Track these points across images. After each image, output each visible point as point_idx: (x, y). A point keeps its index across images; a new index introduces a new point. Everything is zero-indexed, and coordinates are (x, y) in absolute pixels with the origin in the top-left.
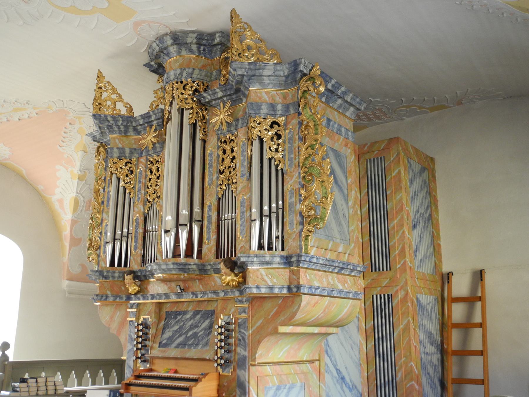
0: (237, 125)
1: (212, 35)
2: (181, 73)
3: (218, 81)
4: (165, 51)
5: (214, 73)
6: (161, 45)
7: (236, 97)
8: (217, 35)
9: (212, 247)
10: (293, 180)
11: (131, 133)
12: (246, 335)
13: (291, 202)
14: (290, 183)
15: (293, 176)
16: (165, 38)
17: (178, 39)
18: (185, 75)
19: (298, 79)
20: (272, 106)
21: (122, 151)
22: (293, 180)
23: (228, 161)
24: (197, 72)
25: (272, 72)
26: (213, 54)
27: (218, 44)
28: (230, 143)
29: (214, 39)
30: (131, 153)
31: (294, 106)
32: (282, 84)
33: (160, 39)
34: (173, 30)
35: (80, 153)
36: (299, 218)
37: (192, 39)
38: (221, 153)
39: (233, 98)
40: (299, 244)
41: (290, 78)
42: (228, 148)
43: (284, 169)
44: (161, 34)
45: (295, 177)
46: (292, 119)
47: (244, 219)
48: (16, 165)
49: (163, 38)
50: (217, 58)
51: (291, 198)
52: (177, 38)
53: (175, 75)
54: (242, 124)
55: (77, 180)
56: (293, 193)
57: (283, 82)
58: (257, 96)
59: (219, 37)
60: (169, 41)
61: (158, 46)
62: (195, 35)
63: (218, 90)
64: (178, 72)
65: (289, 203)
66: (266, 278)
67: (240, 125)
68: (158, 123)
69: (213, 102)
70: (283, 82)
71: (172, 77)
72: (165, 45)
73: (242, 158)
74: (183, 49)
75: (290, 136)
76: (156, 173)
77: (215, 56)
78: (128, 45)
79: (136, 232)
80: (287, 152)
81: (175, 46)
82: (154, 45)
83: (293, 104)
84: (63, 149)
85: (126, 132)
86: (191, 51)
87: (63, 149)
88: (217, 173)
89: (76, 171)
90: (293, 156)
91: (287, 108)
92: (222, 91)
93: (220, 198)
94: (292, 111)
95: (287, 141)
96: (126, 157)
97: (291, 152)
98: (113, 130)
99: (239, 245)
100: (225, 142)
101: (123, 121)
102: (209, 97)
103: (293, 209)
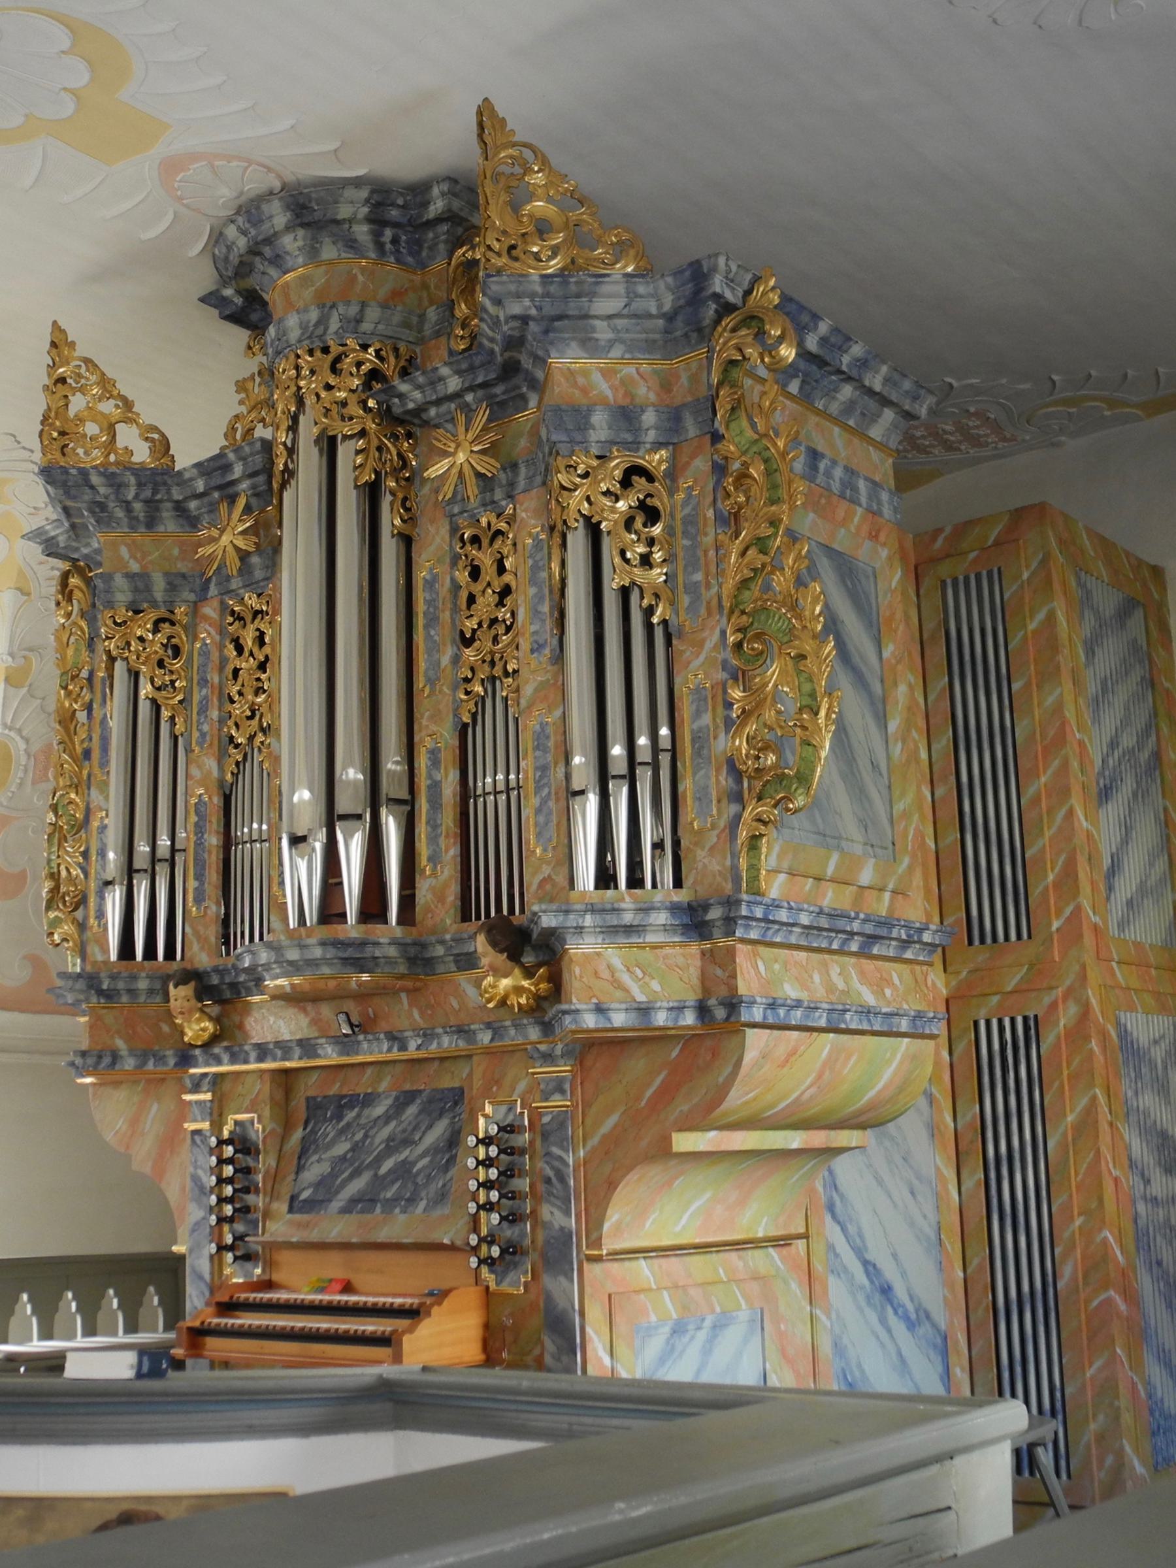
0: (512, 484)
1: (419, 191)
2: (323, 321)
6: (253, 232)
7: (503, 393)
8: (436, 191)
10: (702, 657)
11: (169, 523)
15: (701, 644)
16: (264, 207)
17: (308, 207)
19: (707, 322)
21: (140, 582)
22: (702, 657)
26: (424, 254)
27: (439, 220)
29: (425, 204)
30: (172, 587)
33: (250, 210)
34: (290, 178)
36: (725, 780)
38: (463, 576)
39: (496, 396)
41: (679, 322)
42: (486, 560)
45: (709, 645)
46: (693, 456)
47: (546, 791)
49: (258, 208)
50: (439, 264)
51: (698, 714)
52: (304, 207)
54: (530, 479)
58: (575, 384)
60: (279, 218)
61: (244, 233)
62: (364, 194)
64: (314, 315)
65: (692, 731)
66: (626, 978)
67: (522, 483)
68: (254, 487)
69: (433, 412)
70: (657, 336)
73: (532, 591)
75: (687, 510)
76: (256, 650)
77: (432, 258)
79: (199, 844)
80: (681, 564)
82: (231, 232)
85: (151, 523)
86: (351, 244)
90: (699, 577)
91: (673, 418)
92: (459, 372)
94: (691, 428)
97: (693, 564)
99: (534, 874)
100: (475, 540)
102: (417, 395)
103: (705, 752)
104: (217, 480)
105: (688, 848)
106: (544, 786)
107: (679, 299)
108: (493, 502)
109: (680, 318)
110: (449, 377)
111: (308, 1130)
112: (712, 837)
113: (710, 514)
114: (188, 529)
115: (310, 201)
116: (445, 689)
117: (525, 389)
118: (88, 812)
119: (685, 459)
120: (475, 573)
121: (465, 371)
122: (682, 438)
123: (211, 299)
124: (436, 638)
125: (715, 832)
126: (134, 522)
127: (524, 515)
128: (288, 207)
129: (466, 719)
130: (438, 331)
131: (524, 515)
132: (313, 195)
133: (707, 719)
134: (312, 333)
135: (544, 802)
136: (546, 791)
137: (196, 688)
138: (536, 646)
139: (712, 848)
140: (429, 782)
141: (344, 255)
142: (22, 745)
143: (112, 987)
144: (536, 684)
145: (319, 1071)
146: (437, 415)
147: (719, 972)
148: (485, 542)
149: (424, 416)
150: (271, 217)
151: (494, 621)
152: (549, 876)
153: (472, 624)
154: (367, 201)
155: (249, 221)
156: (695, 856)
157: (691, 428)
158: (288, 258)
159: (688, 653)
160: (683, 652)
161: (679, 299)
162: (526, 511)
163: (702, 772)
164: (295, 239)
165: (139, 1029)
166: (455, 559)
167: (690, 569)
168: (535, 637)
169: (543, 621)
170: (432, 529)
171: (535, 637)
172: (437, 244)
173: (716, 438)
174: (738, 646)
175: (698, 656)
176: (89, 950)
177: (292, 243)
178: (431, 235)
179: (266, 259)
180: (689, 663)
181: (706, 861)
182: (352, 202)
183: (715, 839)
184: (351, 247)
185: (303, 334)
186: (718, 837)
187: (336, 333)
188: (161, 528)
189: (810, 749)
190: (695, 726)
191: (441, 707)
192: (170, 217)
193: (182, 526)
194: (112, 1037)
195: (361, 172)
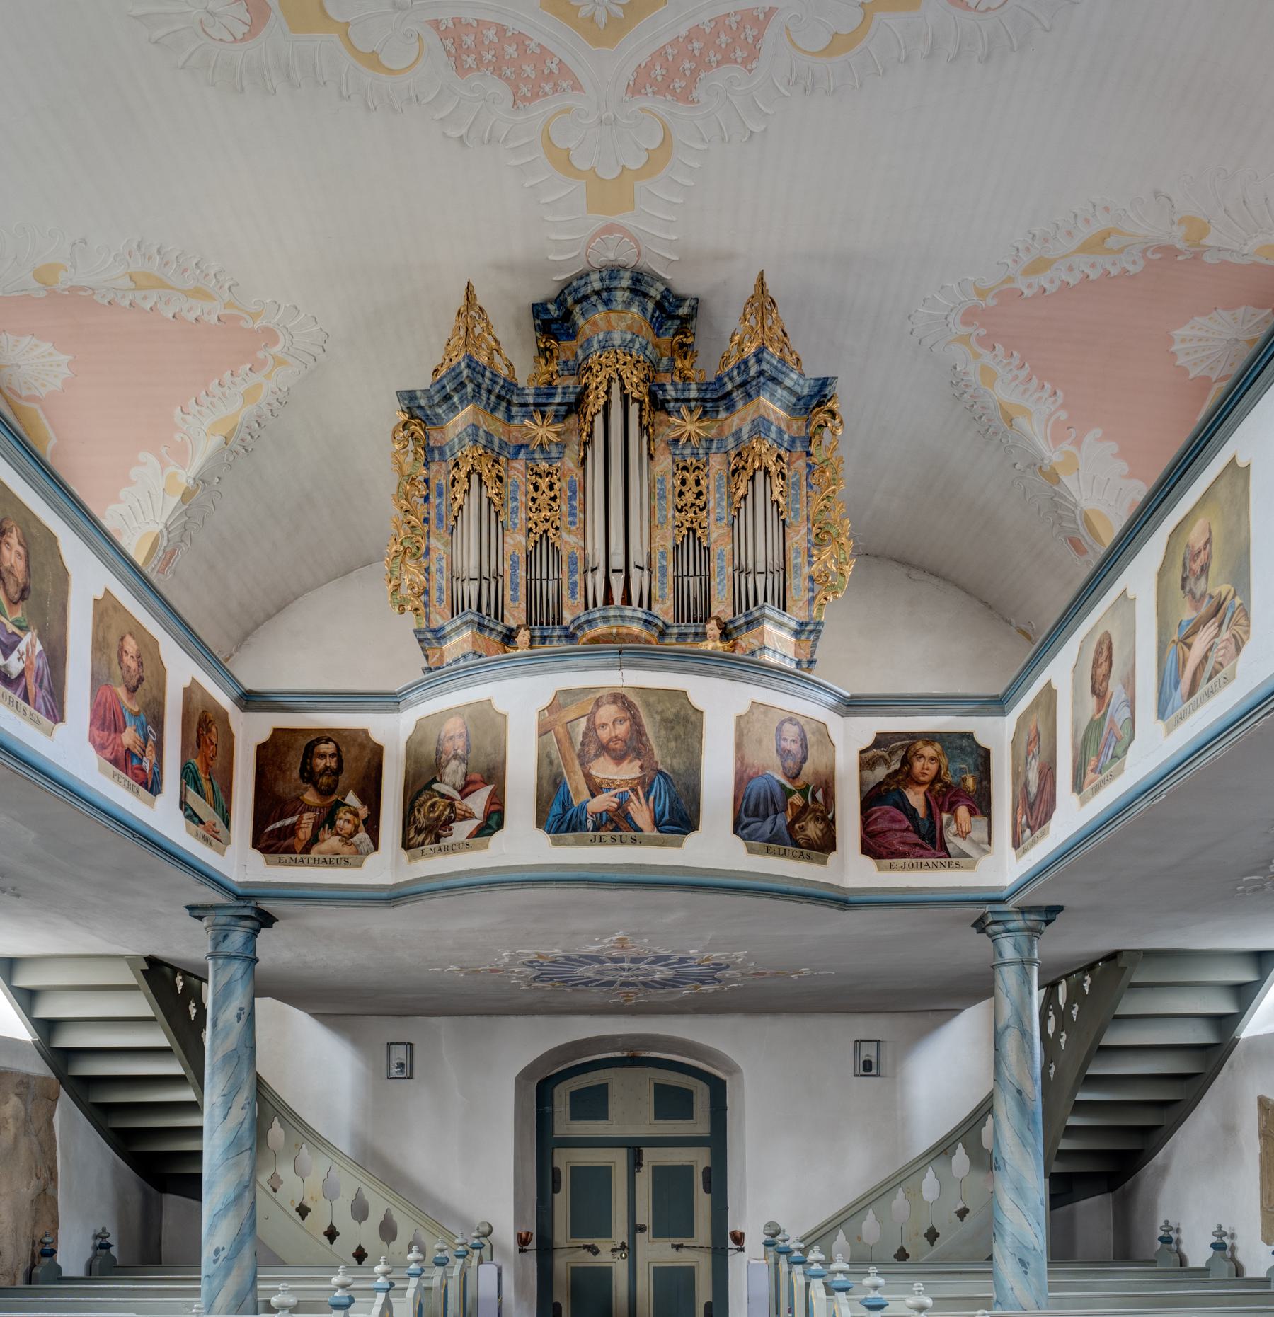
1: (681, 300)
2: (632, 340)
4: (604, 295)
6: (607, 282)
8: (688, 303)
11: (500, 415)
12: (355, 857)
14: (795, 539)
16: (622, 273)
17: (639, 284)
20: (780, 432)
23: (689, 497)
24: (650, 347)
29: (678, 307)
31: (802, 442)
33: (614, 272)
35: (216, 440)
36: (807, 584)
41: (802, 403)
42: (690, 478)
43: (788, 521)
44: (621, 263)
46: (798, 459)
48: (45, 422)
51: (796, 558)
53: (623, 341)
55: (178, 498)
61: (602, 280)
63: (694, 386)
64: (629, 336)
67: (714, 450)
69: (672, 404)
71: (617, 342)
72: (615, 283)
76: (547, 491)
78: (551, 257)
79: (514, 574)
81: (627, 294)
82: (595, 277)
83: (802, 440)
84: (184, 420)
85: (494, 409)
86: (644, 310)
87: (184, 420)
89: (185, 477)
91: (793, 441)
92: (699, 390)
94: (799, 447)
97: (796, 501)
100: (685, 468)
101: (503, 387)
102: (673, 394)
104: (542, 400)
111: (206, 785)
112: (801, 604)
118: (428, 549)
120: (683, 482)
133: (799, 560)
135: (722, 581)
142: (165, 543)
145: (1222, 482)
151: (693, 505)
153: (682, 504)
157: (799, 447)
173: (809, 454)
176: (432, 616)
177: (620, 296)
192: (575, 254)
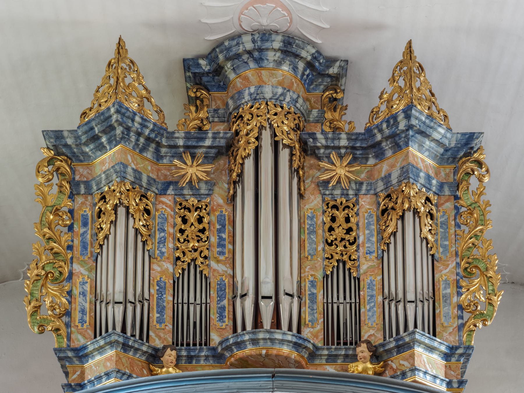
0: (359, 190)
3: (320, 125)
5: (315, 112)
6: (259, 43)
7: (360, 154)
8: (338, 64)
9: (318, 332)
10: (448, 270)
13: (446, 294)
15: (448, 266)
16: (273, 37)
18: (288, 99)
19: (459, 156)
20: (429, 178)
22: (448, 270)
23: (339, 232)
25: (440, 137)
26: (312, 87)
27: (329, 76)
28: (344, 210)
29: (328, 67)
30: (149, 183)
31: (450, 187)
32: (438, 156)
37: (307, 53)
38: (327, 220)
39: (356, 154)
40: (457, 338)
41: (449, 153)
43: (437, 256)
45: (451, 266)
46: (447, 201)
47: (373, 304)
49: (270, 34)
51: (445, 288)
52: (290, 44)
54: (368, 191)
56: (449, 284)
57: (439, 155)
58: (414, 160)
59: (340, 66)
61: (254, 41)
62: (313, 51)
64: (280, 91)
65: (443, 294)
66: (427, 366)
67: (363, 192)
68: (206, 153)
69: (322, 151)
70: (439, 155)
73: (367, 232)
74: (288, 62)
75: (443, 219)
79: (160, 299)
80: (439, 237)
85: (143, 149)
86: (295, 68)
88: (323, 242)
90: (447, 243)
91: (441, 186)
93: (327, 276)
95: (439, 225)
96: (141, 186)
98: (129, 139)
99: (366, 333)
103: (448, 301)
105: (440, 332)
106: (372, 302)
107: (458, 144)
108: (348, 195)
109: (450, 151)
110: (344, 139)
113: (453, 223)
114: (155, 160)
115: (294, 43)
116: (319, 259)
117: (370, 156)
119: (442, 202)
121: (352, 139)
122: (443, 194)
123: (184, 60)
124: (314, 239)
125: (452, 328)
126: (136, 147)
127: (363, 203)
128: (284, 42)
129: (329, 273)
130: (318, 120)
131: (363, 203)
132: (297, 41)
134: (278, 98)
136: (373, 304)
137: (157, 232)
138: (368, 252)
139: (450, 333)
140: (309, 293)
141: (290, 71)
143: (133, 345)
144: (368, 266)
146: (324, 153)
147: (452, 373)
148: (341, 209)
149: (317, 152)
150: (274, 41)
152: (374, 334)
154: (313, 54)
155: (261, 38)
156: (443, 335)
158: (266, 61)
159: (441, 268)
160: (439, 267)
161: (458, 144)
162: (364, 202)
163: (447, 308)
164: (275, 55)
165: (135, 368)
166: (324, 212)
167: (443, 239)
168: (368, 249)
169: (373, 244)
170: (312, 197)
171: (368, 249)
172: (320, 85)
174: (466, 269)
175: (446, 269)
178: (320, 80)
179: (253, 57)
180: (442, 271)
181: (448, 337)
182: (308, 52)
183: (452, 330)
184: (294, 70)
185: (273, 96)
186: (453, 330)
187: (288, 103)
188: (145, 154)
189: (492, 307)
190: (444, 292)
191: (317, 265)
193: (154, 157)
194: (125, 368)
195: (319, 41)
